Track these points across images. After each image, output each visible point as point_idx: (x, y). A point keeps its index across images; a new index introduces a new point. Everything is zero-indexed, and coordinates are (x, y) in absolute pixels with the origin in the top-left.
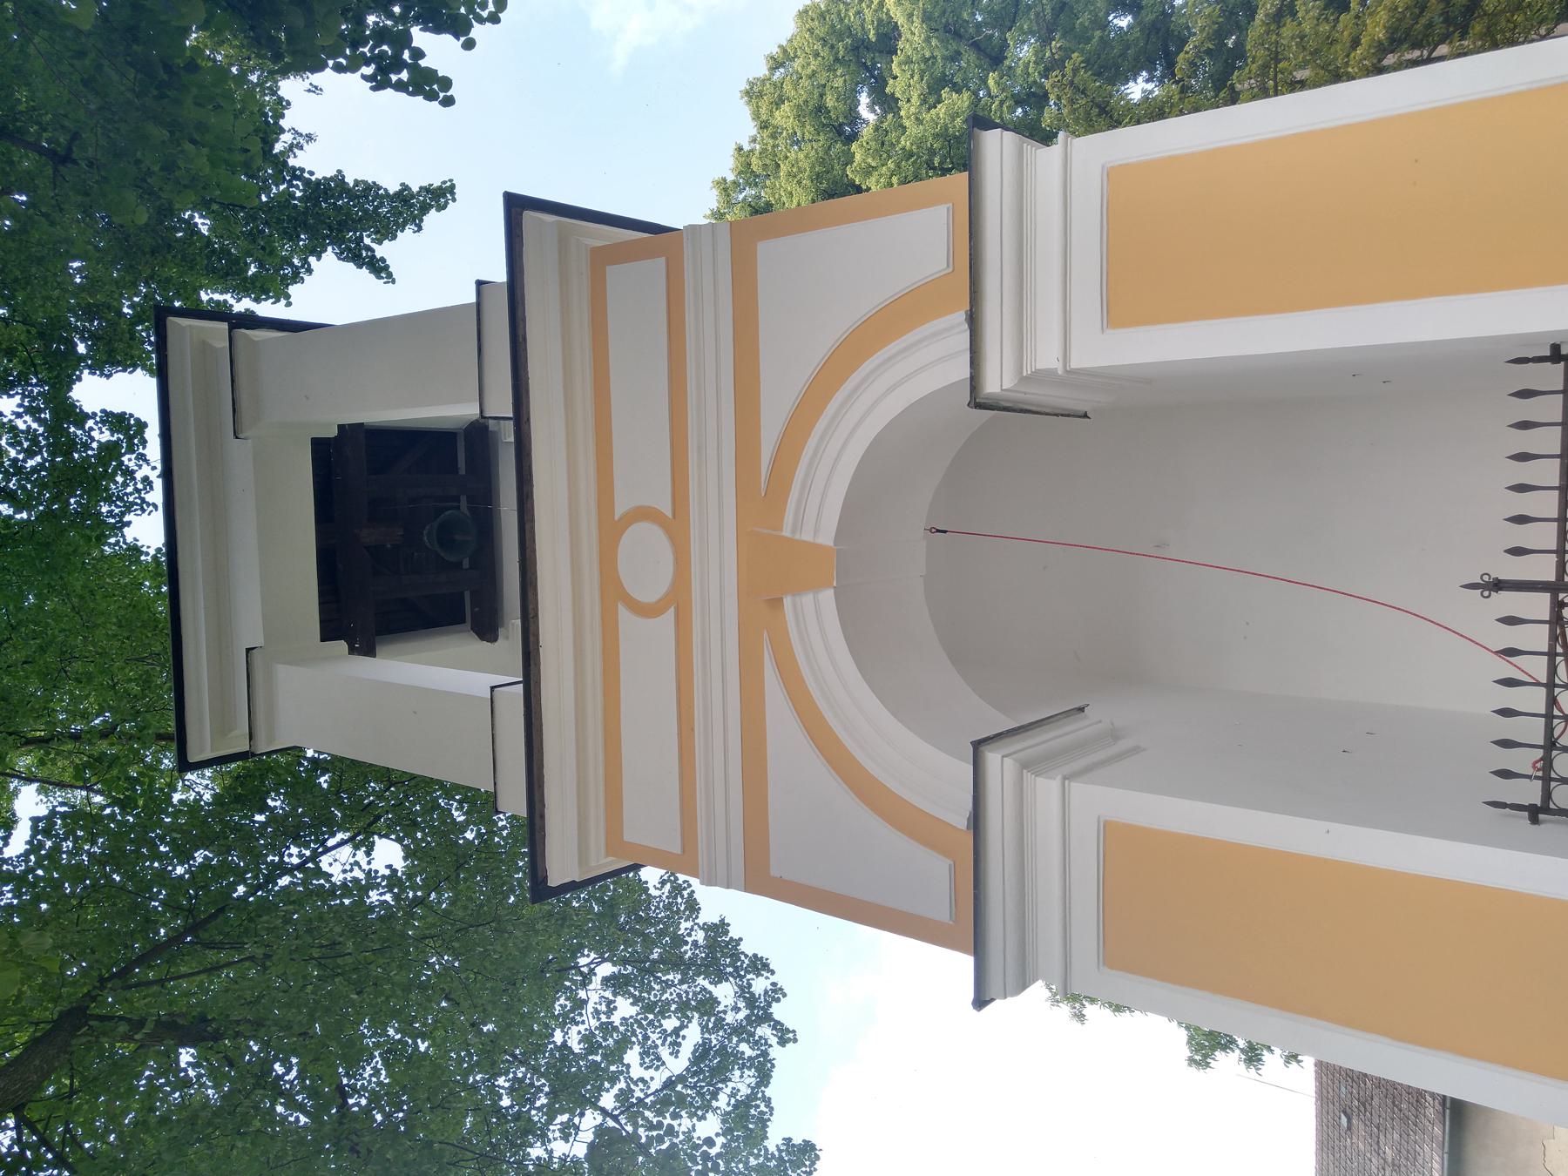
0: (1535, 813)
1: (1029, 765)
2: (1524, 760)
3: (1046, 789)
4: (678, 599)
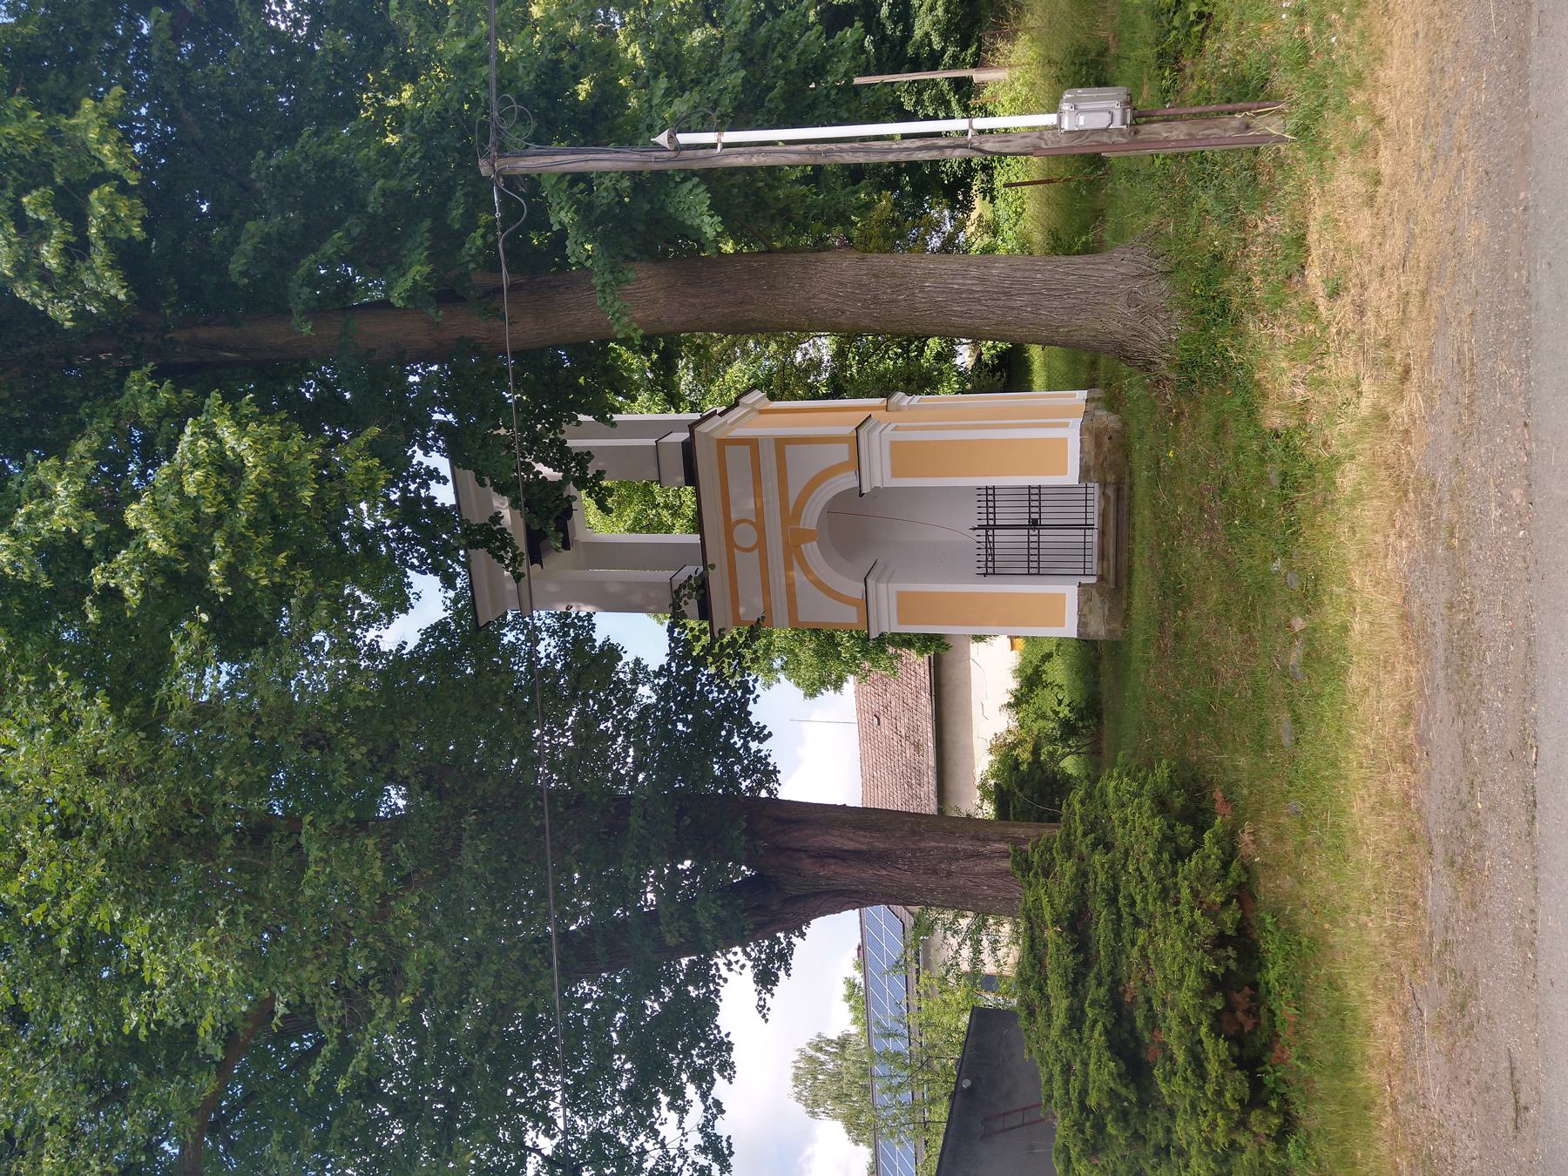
0: (985, 575)
1: (877, 581)
2: (982, 564)
3: (882, 587)
4: (761, 545)
